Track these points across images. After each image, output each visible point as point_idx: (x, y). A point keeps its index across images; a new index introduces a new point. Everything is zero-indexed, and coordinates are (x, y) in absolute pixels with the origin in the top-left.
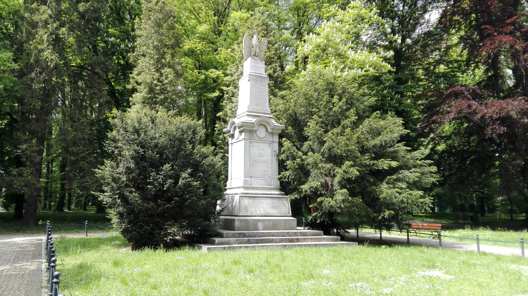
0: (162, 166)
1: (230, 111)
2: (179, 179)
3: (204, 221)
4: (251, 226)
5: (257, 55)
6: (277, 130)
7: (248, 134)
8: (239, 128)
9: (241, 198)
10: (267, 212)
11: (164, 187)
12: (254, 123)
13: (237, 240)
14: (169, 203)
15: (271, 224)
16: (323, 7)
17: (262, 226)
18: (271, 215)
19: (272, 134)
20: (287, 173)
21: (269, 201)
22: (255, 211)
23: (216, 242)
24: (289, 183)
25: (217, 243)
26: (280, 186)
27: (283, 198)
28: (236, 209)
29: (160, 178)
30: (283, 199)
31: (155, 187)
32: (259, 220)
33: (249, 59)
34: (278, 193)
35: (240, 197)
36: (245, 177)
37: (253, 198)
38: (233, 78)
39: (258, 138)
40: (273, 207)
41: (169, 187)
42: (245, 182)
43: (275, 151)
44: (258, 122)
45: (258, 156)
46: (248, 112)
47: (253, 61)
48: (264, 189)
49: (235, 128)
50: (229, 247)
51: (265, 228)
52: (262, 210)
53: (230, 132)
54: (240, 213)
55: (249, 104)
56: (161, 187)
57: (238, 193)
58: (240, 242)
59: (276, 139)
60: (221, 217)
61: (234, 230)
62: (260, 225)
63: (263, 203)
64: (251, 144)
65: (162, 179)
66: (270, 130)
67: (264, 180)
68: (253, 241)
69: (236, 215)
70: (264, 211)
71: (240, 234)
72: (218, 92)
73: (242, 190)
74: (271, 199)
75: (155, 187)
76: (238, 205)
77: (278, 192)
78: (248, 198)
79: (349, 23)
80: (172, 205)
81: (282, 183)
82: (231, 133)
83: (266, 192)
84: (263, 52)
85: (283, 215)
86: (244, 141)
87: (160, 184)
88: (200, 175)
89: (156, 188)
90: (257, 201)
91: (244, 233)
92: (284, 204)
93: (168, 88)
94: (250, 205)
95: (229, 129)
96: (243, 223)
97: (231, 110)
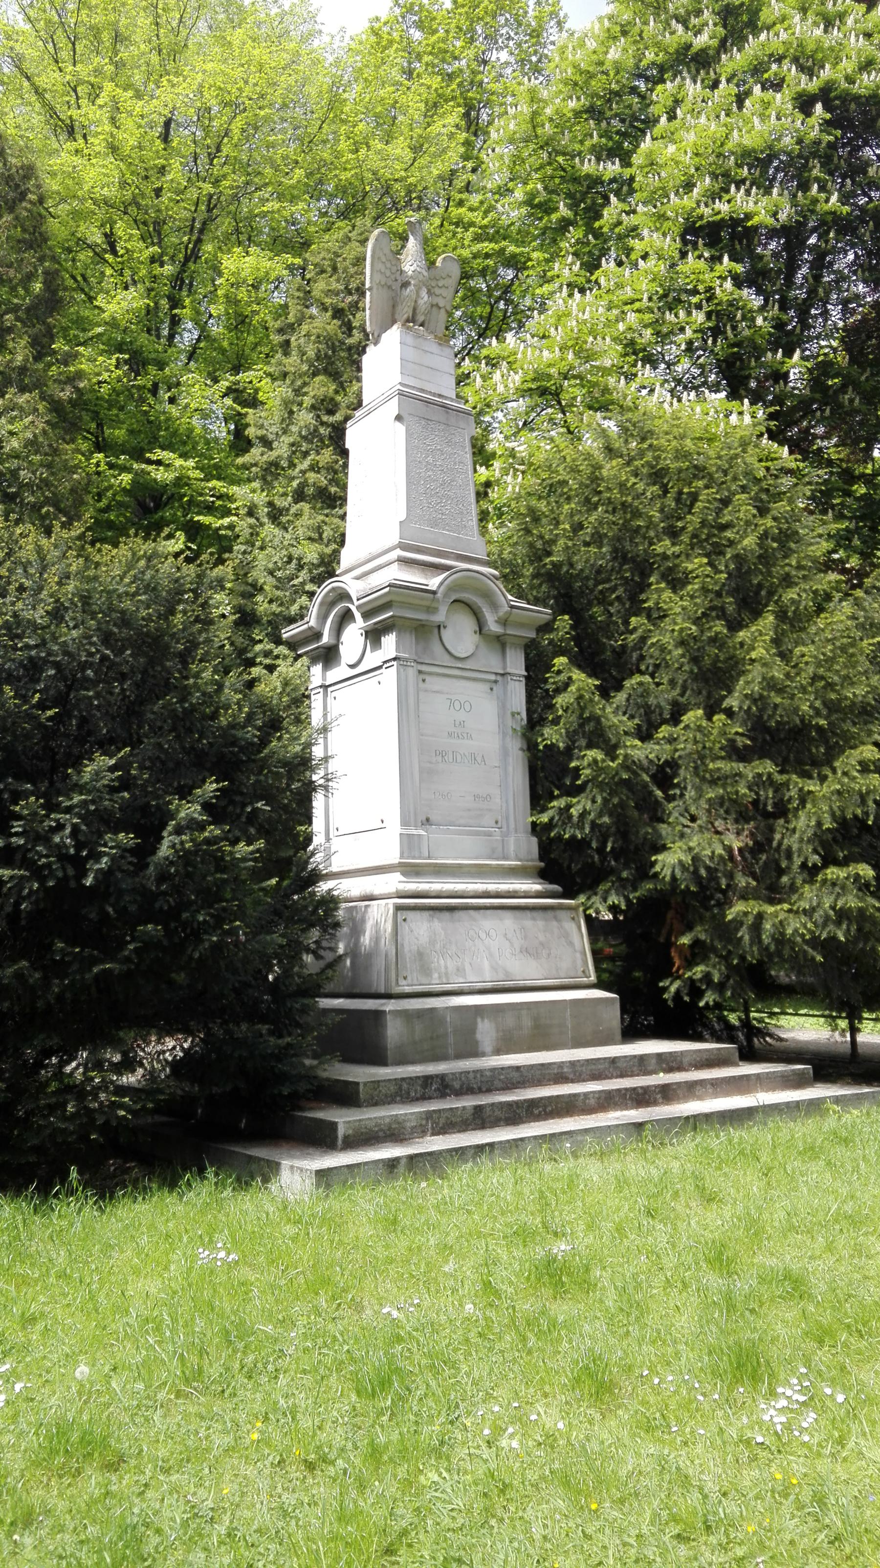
0: (77, 763)
1: (270, 580)
2: (163, 826)
3: (271, 1033)
4: (451, 1039)
5: (421, 318)
6: (522, 625)
7: (410, 639)
8: (366, 616)
9: (401, 915)
10: (507, 973)
11: (84, 874)
12: (434, 593)
13: (429, 1115)
14: (111, 950)
15: (527, 1022)
16: (530, 264)
17: (494, 1034)
18: (522, 983)
19: (500, 643)
20: (579, 805)
21: (508, 921)
22: (460, 971)
23: (341, 1131)
24: (577, 845)
25: (346, 1138)
26: (541, 858)
27: (561, 907)
28: (379, 964)
29: (60, 827)
30: (562, 914)
31: (38, 873)
32: (479, 1010)
33: (393, 336)
34: (537, 887)
35: (398, 908)
36: (405, 823)
37: (446, 915)
38: (273, 454)
39: (447, 660)
40: (526, 951)
41: (106, 875)
42: (408, 843)
43: (513, 714)
44: (451, 589)
45: (450, 735)
46: (402, 546)
47: (410, 340)
48: (480, 872)
49: (346, 617)
50: (411, 1158)
51: (506, 1046)
52: (486, 965)
53: (318, 635)
54: (402, 982)
55: (403, 516)
56: (71, 872)
57: (377, 892)
58: (442, 1121)
59: (516, 664)
60: (326, 1003)
61: (380, 1060)
62: (486, 1032)
63: (488, 934)
64: (421, 684)
65: (75, 829)
66: (493, 627)
67: (477, 834)
68: (498, 1113)
69: (382, 990)
70: (494, 969)
71: (427, 1080)
72: (183, 538)
73: (394, 882)
74: (518, 913)
75: (38, 873)
76: (386, 944)
77: (537, 887)
78: (426, 914)
79: (637, 305)
80: (128, 960)
81: (545, 850)
82: (326, 639)
83: (492, 886)
84: (443, 311)
85: (566, 981)
86: (394, 670)
87: (63, 857)
88: (255, 811)
89: (42, 880)
90: (464, 923)
91: (442, 1077)
92: (566, 935)
93: (22, 473)
94: (438, 946)
95: (313, 623)
96: (419, 1029)
97: (271, 573)
